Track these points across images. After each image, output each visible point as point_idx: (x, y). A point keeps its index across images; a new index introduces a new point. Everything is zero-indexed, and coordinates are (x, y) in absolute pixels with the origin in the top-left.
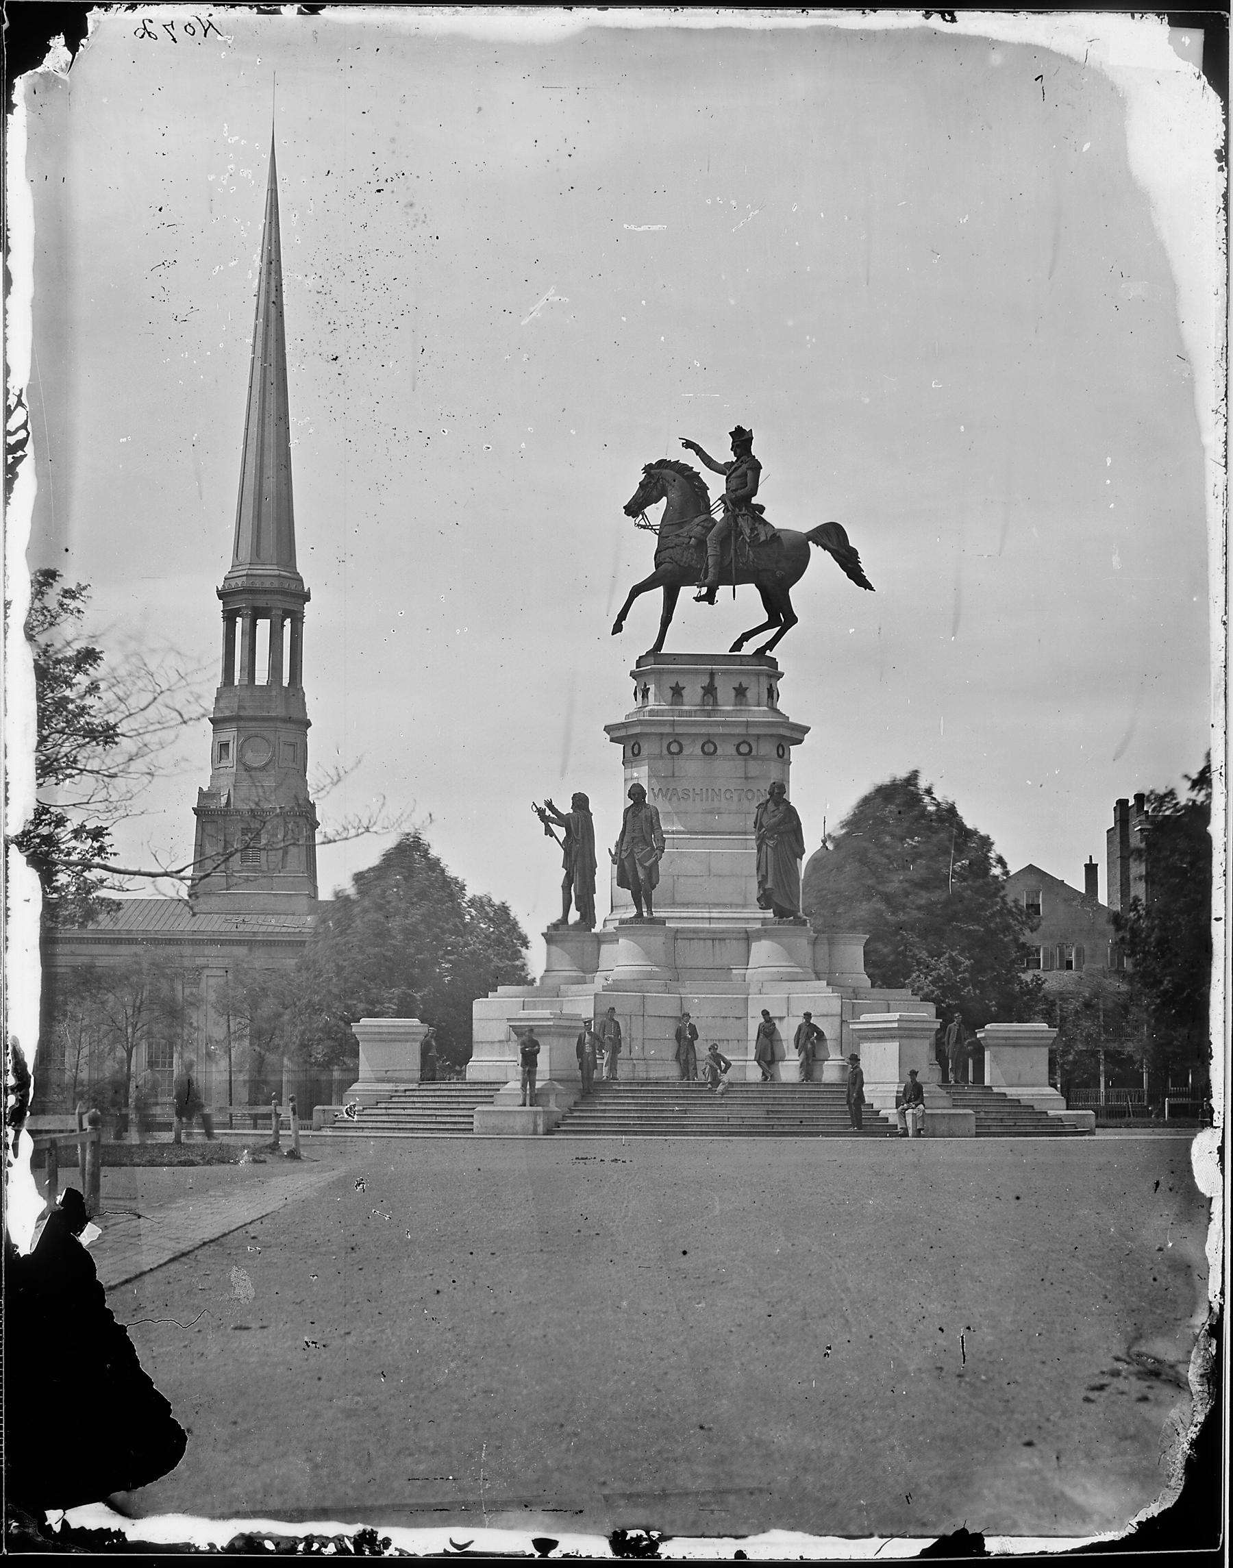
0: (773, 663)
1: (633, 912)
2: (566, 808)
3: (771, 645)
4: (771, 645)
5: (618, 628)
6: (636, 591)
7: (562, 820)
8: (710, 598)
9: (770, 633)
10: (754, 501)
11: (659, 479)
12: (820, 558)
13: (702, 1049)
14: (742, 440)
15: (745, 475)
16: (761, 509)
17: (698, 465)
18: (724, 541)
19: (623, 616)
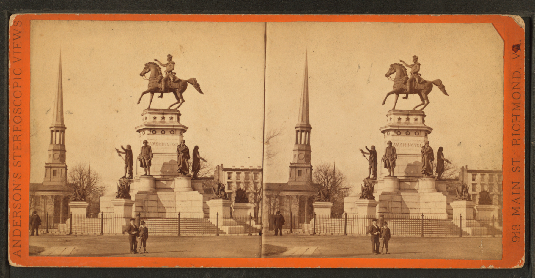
0: (423, 112)
1: (388, 174)
2: (125, 148)
3: (178, 107)
4: (178, 107)
5: (384, 103)
6: (389, 94)
7: (126, 150)
8: (406, 98)
9: (423, 106)
10: (419, 73)
11: (393, 67)
12: (435, 88)
13: (293, 215)
14: (416, 59)
15: (416, 67)
16: (420, 75)
17: (156, 62)
18: (411, 82)
19: (140, 99)
